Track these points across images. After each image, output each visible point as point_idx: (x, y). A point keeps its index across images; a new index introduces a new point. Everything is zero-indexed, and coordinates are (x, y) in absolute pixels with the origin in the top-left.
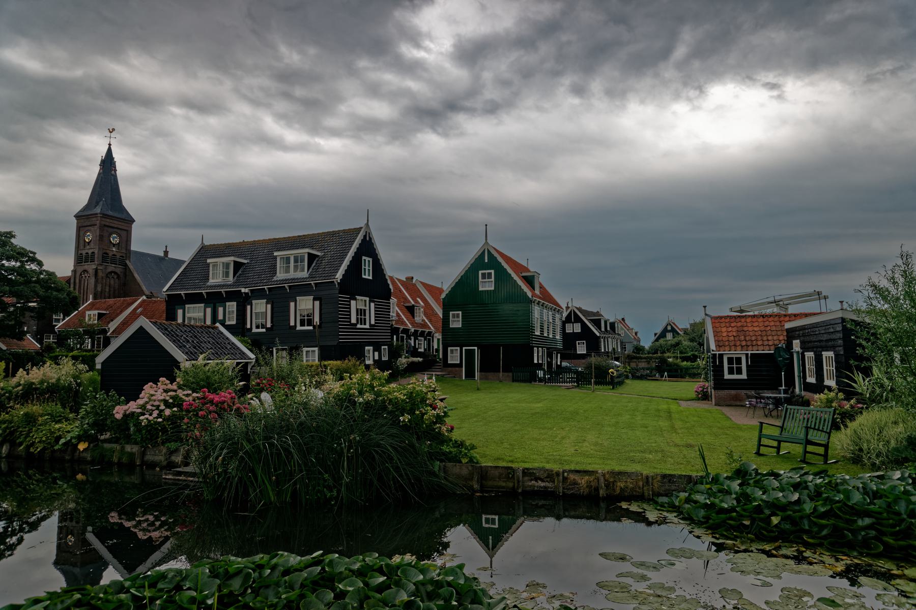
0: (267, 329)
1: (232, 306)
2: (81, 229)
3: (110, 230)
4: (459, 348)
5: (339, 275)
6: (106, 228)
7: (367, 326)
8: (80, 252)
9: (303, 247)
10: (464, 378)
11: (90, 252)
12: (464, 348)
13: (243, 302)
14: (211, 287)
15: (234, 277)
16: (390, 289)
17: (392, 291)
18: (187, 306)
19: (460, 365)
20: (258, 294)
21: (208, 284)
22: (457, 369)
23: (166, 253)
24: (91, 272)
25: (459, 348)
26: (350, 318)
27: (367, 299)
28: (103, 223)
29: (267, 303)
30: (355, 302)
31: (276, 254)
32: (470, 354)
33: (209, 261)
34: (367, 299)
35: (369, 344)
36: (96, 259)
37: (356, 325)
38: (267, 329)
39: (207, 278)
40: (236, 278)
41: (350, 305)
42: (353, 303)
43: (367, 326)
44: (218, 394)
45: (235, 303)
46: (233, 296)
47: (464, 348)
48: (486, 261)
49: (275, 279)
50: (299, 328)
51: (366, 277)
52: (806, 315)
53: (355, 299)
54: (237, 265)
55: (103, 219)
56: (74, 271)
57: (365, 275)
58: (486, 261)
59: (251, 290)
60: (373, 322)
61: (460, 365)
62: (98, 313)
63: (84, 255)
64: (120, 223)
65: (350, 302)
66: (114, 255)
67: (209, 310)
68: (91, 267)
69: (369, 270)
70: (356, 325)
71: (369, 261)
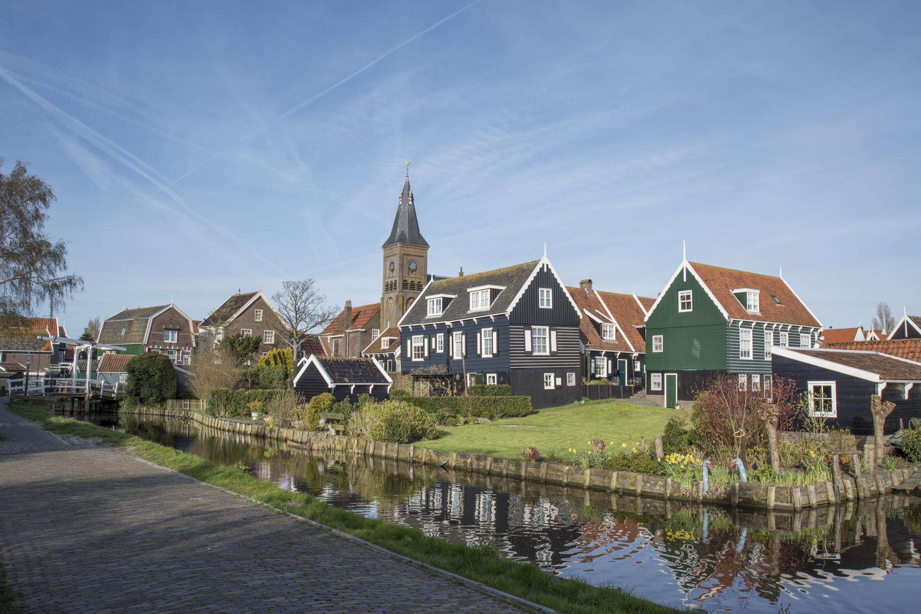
0: (425, 358)
1: (440, 336)
2: (387, 259)
3: (409, 258)
4: (661, 374)
5: (510, 309)
6: (405, 256)
7: (548, 353)
8: (387, 280)
9: (439, 293)
10: (665, 407)
11: (393, 280)
12: (665, 374)
13: (448, 332)
14: (429, 320)
15: (443, 311)
16: (579, 316)
17: (581, 318)
18: (413, 337)
19: (661, 393)
20: (457, 326)
21: (427, 318)
22: (660, 396)
23: (461, 274)
24: (394, 298)
25: (661, 374)
26: (524, 347)
27: (547, 328)
28: (403, 252)
29: (424, 338)
30: (530, 331)
31: (469, 290)
32: (671, 380)
33: (469, 290)
34: (547, 328)
35: (550, 371)
36: (397, 287)
37: (532, 352)
38: (425, 358)
39: (425, 313)
40: (444, 312)
41: (524, 335)
42: (528, 333)
43: (548, 353)
44: (205, 382)
45: (442, 334)
46: (442, 328)
47: (665, 374)
48: (685, 280)
49: (469, 312)
50: (414, 360)
51: (545, 307)
52: (792, 350)
53: (531, 329)
54: (446, 301)
55: (403, 249)
56: (382, 299)
57: (543, 304)
58: (685, 280)
59: (453, 323)
60: (554, 349)
61: (662, 393)
62: (390, 339)
63: (393, 282)
64: (418, 250)
65: (524, 332)
66: (412, 282)
67: (426, 340)
68: (393, 294)
69: (548, 300)
70: (532, 352)
71: (548, 292)
